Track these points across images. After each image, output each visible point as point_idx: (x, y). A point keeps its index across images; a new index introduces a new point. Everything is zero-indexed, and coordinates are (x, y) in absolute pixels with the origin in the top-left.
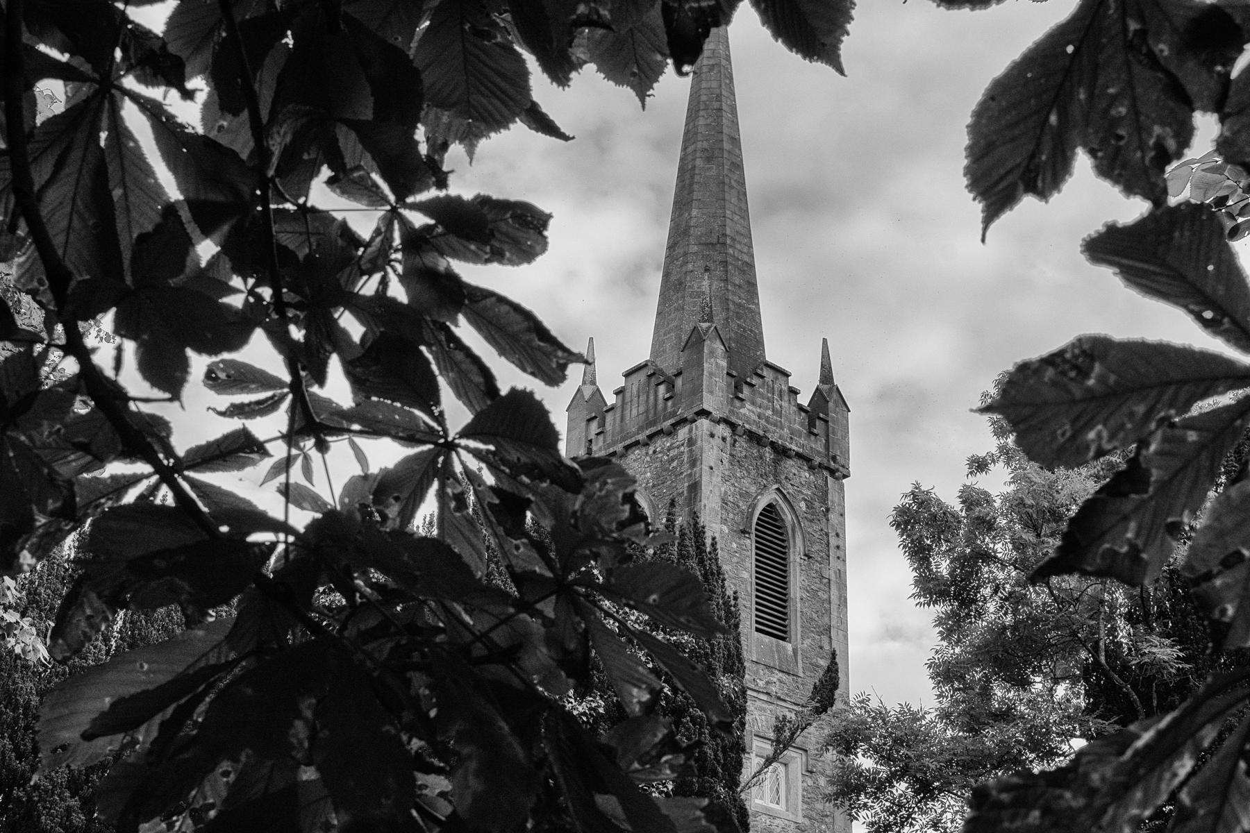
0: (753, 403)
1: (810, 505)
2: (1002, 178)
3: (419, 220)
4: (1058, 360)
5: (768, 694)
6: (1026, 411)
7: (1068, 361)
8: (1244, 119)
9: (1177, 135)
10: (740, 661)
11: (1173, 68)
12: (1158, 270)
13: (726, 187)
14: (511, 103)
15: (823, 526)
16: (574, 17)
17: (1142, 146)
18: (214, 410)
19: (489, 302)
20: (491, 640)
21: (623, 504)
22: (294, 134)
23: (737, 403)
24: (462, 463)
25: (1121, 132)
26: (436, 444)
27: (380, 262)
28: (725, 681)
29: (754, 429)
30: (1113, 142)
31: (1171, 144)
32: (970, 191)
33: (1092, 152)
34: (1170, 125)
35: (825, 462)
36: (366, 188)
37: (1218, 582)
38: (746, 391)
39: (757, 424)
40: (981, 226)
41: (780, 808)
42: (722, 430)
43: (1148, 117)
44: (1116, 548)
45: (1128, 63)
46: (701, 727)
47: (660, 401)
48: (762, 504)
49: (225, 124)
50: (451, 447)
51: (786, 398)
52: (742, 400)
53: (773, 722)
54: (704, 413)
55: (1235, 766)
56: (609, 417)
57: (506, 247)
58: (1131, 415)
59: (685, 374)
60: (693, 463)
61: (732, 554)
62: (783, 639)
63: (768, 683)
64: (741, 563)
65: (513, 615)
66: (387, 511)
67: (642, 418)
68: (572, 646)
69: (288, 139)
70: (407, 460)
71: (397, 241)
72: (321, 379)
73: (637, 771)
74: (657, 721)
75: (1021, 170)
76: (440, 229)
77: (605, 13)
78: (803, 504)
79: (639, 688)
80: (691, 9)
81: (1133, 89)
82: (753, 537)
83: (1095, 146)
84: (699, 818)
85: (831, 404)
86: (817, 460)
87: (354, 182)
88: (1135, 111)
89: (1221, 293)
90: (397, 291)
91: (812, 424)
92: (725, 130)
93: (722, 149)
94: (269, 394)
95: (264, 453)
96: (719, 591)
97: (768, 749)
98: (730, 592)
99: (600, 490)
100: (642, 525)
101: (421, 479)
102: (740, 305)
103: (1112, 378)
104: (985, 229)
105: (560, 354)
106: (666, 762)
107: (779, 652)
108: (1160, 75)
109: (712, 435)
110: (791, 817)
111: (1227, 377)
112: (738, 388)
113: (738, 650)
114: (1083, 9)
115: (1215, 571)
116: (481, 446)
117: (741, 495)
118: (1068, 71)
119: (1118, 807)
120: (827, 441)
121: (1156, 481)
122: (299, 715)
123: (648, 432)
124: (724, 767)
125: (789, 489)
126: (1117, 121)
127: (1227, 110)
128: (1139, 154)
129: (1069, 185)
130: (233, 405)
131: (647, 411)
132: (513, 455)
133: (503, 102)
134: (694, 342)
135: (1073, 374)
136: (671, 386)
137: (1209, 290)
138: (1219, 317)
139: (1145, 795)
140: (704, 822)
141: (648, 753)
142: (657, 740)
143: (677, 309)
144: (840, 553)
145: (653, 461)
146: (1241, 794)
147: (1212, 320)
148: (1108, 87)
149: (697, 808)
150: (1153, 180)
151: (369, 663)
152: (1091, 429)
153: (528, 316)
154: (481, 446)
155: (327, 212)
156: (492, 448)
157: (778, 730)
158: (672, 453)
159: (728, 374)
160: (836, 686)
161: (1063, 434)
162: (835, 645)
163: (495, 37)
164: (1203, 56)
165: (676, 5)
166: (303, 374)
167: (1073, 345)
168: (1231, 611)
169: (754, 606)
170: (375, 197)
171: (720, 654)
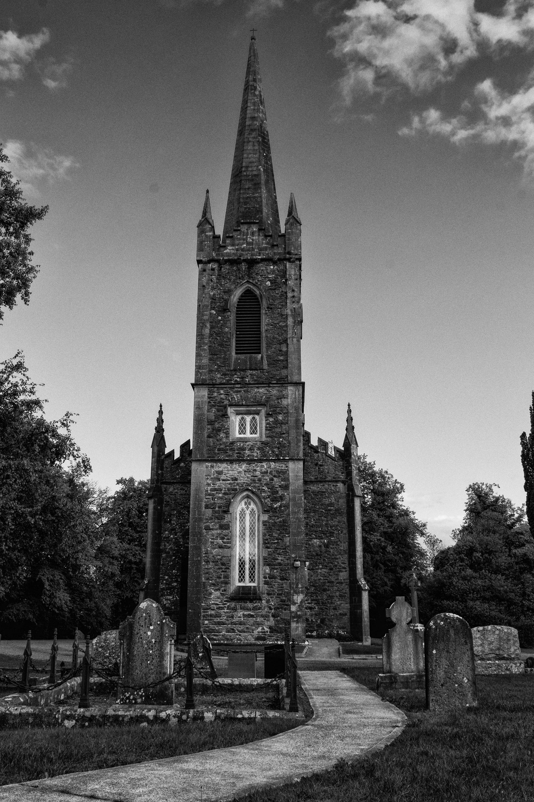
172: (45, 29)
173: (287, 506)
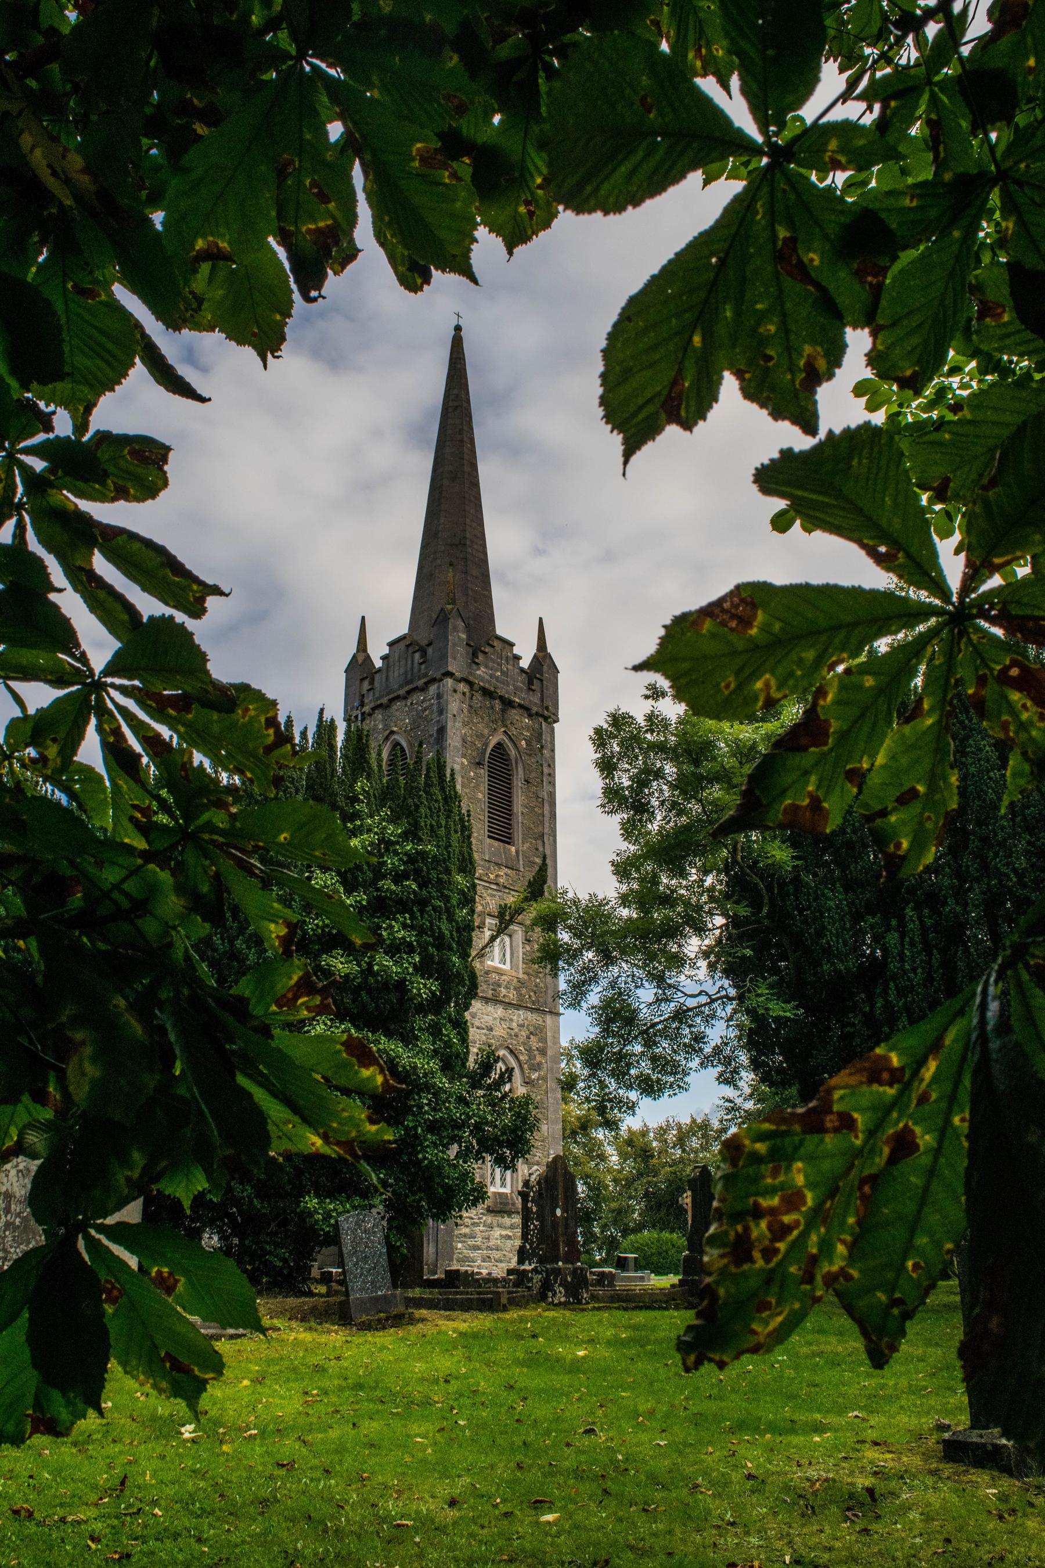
0: (486, 667)
1: (529, 743)
2: (641, 408)
6: (686, 665)
9: (827, 354)
17: (792, 369)
19: (120, 540)
23: (474, 667)
25: (771, 352)
26: (84, 684)
31: (821, 364)
32: (607, 423)
33: (739, 374)
35: (540, 711)
38: (481, 658)
39: (489, 682)
41: (507, 967)
42: (462, 687)
45: (777, 276)
47: (416, 665)
48: (493, 741)
50: (99, 687)
56: (377, 677)
57: (129, 485)
60: (441, 711)
66: (46, 753)
70: (58, 701)
73: (275, 1013)
74: (292, 965)
75: (663, 398)
77: (224, 245)
78: (523, 743)
80: (309, 231)
81: (782, 304)
83: (742, 367)
85: (545, 668)
86: (535, 709)
88: (785, 329)
98: (464, 811)
104: (626, 463)
105: (195, 587)
106: (303, 1004)
108: (811, 288)
109: (455, 691)
112: (475, 655)
116: (126, 682)
118: (713, 285)
123: (407, 688)
124: (458, 943)
125: (513, 731)
126: (763, 341)
128: (789, 377)
129: (716, 413)
131: (406, 673)
134: (442, 620)
136: (424, 654)
142: (292, 982)
145: (411, 710)
148: (756, 303)
153: (160, 551)
154: (126, 682)
160: (545, 882)
163: (100, 295)
165: (292, 228)
172: (439, 144)
173: (544, 1079)
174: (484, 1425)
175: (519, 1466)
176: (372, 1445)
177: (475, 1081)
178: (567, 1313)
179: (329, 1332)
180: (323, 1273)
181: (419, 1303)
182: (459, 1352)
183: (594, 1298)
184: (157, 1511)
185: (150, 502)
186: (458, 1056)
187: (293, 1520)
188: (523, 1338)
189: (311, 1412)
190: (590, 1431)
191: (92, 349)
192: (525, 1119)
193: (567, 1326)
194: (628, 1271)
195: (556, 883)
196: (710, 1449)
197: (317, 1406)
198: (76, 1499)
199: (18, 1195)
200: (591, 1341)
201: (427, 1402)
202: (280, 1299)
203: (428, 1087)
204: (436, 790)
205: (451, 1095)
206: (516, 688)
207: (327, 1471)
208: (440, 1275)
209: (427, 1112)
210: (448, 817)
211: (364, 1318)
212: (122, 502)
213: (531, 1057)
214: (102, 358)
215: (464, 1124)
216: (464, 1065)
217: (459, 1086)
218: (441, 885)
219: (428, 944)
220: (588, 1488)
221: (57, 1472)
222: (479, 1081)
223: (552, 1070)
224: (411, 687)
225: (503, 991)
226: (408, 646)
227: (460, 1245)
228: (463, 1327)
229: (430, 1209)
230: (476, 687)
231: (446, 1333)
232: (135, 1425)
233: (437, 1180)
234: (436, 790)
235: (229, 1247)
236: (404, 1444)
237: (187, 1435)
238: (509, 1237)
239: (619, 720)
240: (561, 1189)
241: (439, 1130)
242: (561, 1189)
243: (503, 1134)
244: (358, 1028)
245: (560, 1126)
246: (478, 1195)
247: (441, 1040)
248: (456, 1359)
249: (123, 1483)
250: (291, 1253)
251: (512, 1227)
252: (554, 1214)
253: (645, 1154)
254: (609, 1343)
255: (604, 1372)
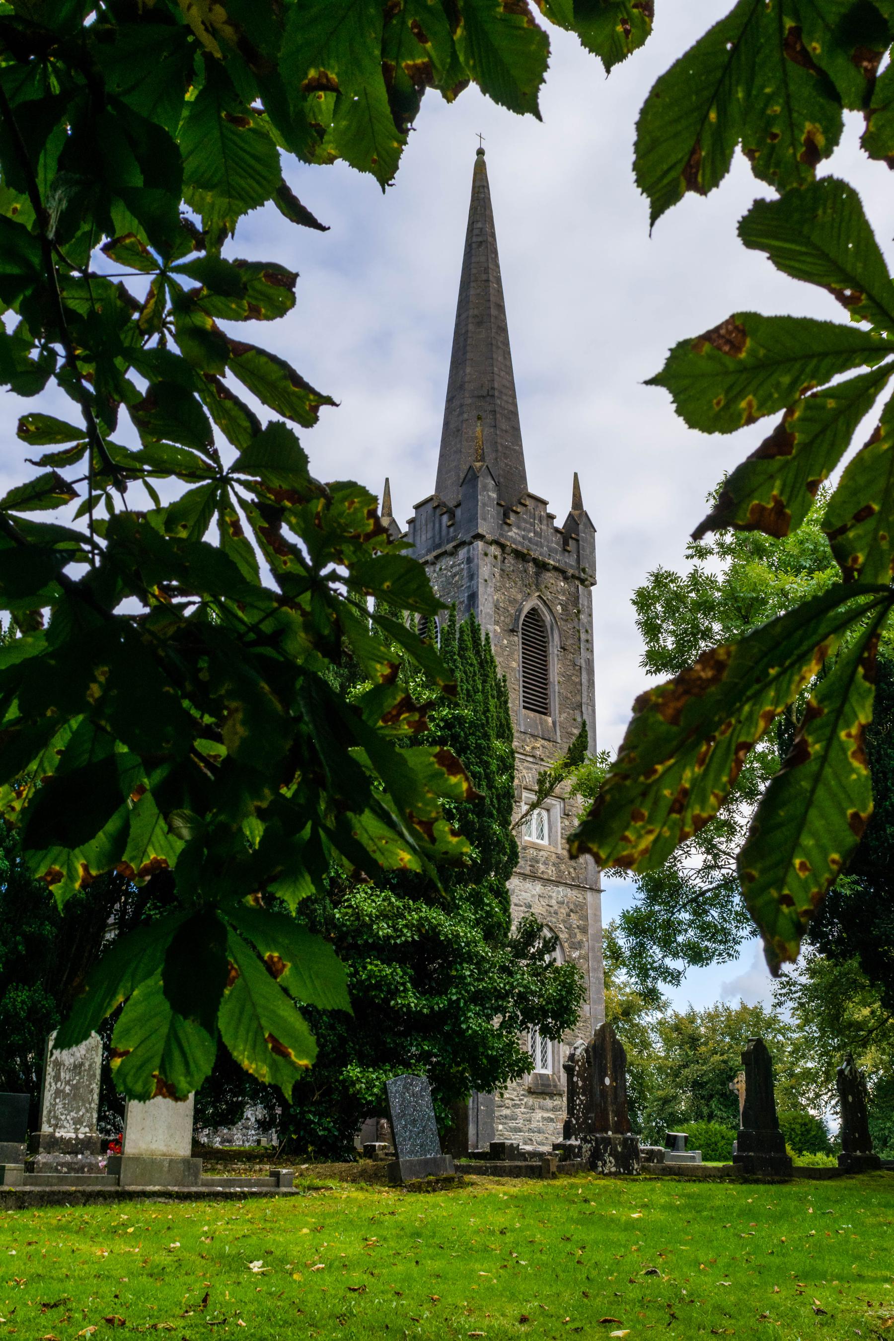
0: (519, 528)
1: (565, 608)
2: (666, 173)
3: (188, 283)
4: (714, 336)
5: (533, 756)
6: (686, 382)
7: (723, 337)
8: (889, 114)
9: (825, 132)
10: (510, 729)
11: (824, 65)
12: (804, 249)
13: (494, 348)
14: (264, 183)
15: (575, 624)
16: (306, 81)
17: (794, 143)
18: (30, 461)
20: (260, 630)
21: (368, 518)
22: (70, 201)
23: (506, 528)
24: (236, 494)
25: (776, 130)
26: (214, 479)
27: (156, 321)
28: (497, 743)
29: (519, 548)
30: (769, 141)
31: (820, 140)
34: (820, 121)
35: (577, 573)
36: (138, 254)
37: (851, 534)
38: (512, 518)
39: (522, 544)
40: (649, 221)
41: (545, 842)
42: (494, 550)
43: (800, 114)
44: (764, 504)
45: (783, 60)
46: (480, 780)
49: (18, 206)
50: (225, 481)
51: (545, 522)
52: (509, 525)
53: (537, 777)
54: (480, 537)
55: (854, 671)
57: (261, 304)
58: (778, 385)
59: (463, 506)
60: (472, 576)
61: (503, 648)
62: (545, 714)
63: (533, 748)
64: (510, 655)
65: (276, 609)
67: (430, 542)
68: (326, 632)
69: (64, 205)
70: (190, 493)
71: (169, 306)
72: (112, 425)
73: (382, 728)
76: (205, 292)
77: (333, 76)
78: (559, 608)
79: (382, 664)
80: (408, 66)
82: (520, 634)
83: (753, 147)
84: (431, 764)
85: (581, 526)
86: (571, 572)
87: (126, 248)
88: (788, 108)
89: (859, 270)
90: (173, 346)
91: (566, 543)
92: (492, 298)
93: (489, 315)
94: (74, 444)
95: (75, 494)
96: (492, 675)
97: (534, 797)
98: (499, 676)
99: (349, 508)
100: (385, 536)
101: (203, 510)
102: (507, 447)
103: (762, 352)
104: (652, 225)
105: (312, 397)
107: (541, 724)
108: (811, 71)
109: (486, 555)
110: (553, 849)
111: (863, 350)
112: (506, 515)
113: (507, 720)
114: (738, 6)
115: (849, 524)
116: (250, 478)
117: (510, 602)
118: (727, 68)
119: (754, 705)
120: (578, 556)
121: (798, 444)
122: (94, 680)
123: (435, 553)
125: (548, 596)
126: (770, 121)
127: (873, 106)
128: (791, 151)
129: (727, 181)
130: (45, 456)
131: (433, 537)
132: (276, 483)
133: (258, 183)
134: (470, 479)
135: (726, 348)
136: (452, 515)
137: (849, 268)
138: (857, 294)
139: (778, 691)
140: (436, 766)
141: (390, 713)
142: (396, 702)
143: (456, 452)
144: (588, 646)
146: (859, 694)
147: (851, 297)
149: (430, 754)
150: (803, 175)
151: (155, 642)
152: (743, 399)
153: (283, 365)
154: (250, 478)
155: (104, 277)
156: (258, 479)
157: (541, 782)
158: (454, 570)
159: (498, 504)
160: (585, 748)
161: (718, 403)
162: (585, 717)
163: (248, 123)
164: (852, 52)
165: (393, 63)
166: (97, 421)
167: (727, 322)
168: (861, 559)
169: (522, 689)
170: (146, 265)
171: (494, 723)
173: (586, 958)
174: (545, 1265)
175: (585, 1295)
176: (438, 1276)
177: (520, 951)
178: (619, 1182)
179: (380, 1192)
180: (366, 1147)
181: (467, 1170)
182: (512, 1211)
183: (644, 1169)
184: (240, 1321)
185: (278, 320)
186: (500, 925)
187: (372, 1328)
188: (574, 1202)
189: (373, 1254)
190: (652, 1273)
191: (245, 171)
192: (570, 992)
193: (620, 1193)
194: (678, 1150)
195: (595, 750)
196: (776, 1289)
197: (378, 1249)
198: (163, 1313)
199: (67, 1063)
200: (645, 1206)
201: (486, 1249)
202: (329, 1164)
203: (469, 958)
204: (470, 654)
205: (493, 965)
206: (551, 550)
207: (398, 1294)
208: (484, 1147)
209: (470, 984)
210: (484, 682)
211: (414, 1180)
212: (253, 321)
213: (572, 935)
214: (254, 179)
215: (508, 993)
216: (506, 935)
217: (503, 955)
218: (481, 751)
219: (468, 811)
220: (652, 1315)
221: (138, 1294)
222: (523, 949)
223: (593, 949)
224: (439, 551)
225: (542, 867)
226: (435, 508)
227: (500, 1127)
228: (514, 1191)
229: (474, 1081)
230: (508, 550)
231: (496, 1196)
232: (204, 1262)
233: (481, 1050)
234: (470, 654)
235: (273, 1116)
236: (470, 1275)
237: (256, 1270)
238: (551, 1120)
239: (660, 579)
240: (609, 1057)
241: (482, 999)
242: (609, 1057)
243: (548, 1003)
244: (399, 897)
245: (603, 1006)
246: (524, 1065)
247: (482, 909)
248: (509, 1217)
249: (205, 1300)
250: (335, 1122)
251: (554, 1109)
252: (603, 1083)
253: (693, 1041)
254: (664, 1208)
255: (661, 1230)
